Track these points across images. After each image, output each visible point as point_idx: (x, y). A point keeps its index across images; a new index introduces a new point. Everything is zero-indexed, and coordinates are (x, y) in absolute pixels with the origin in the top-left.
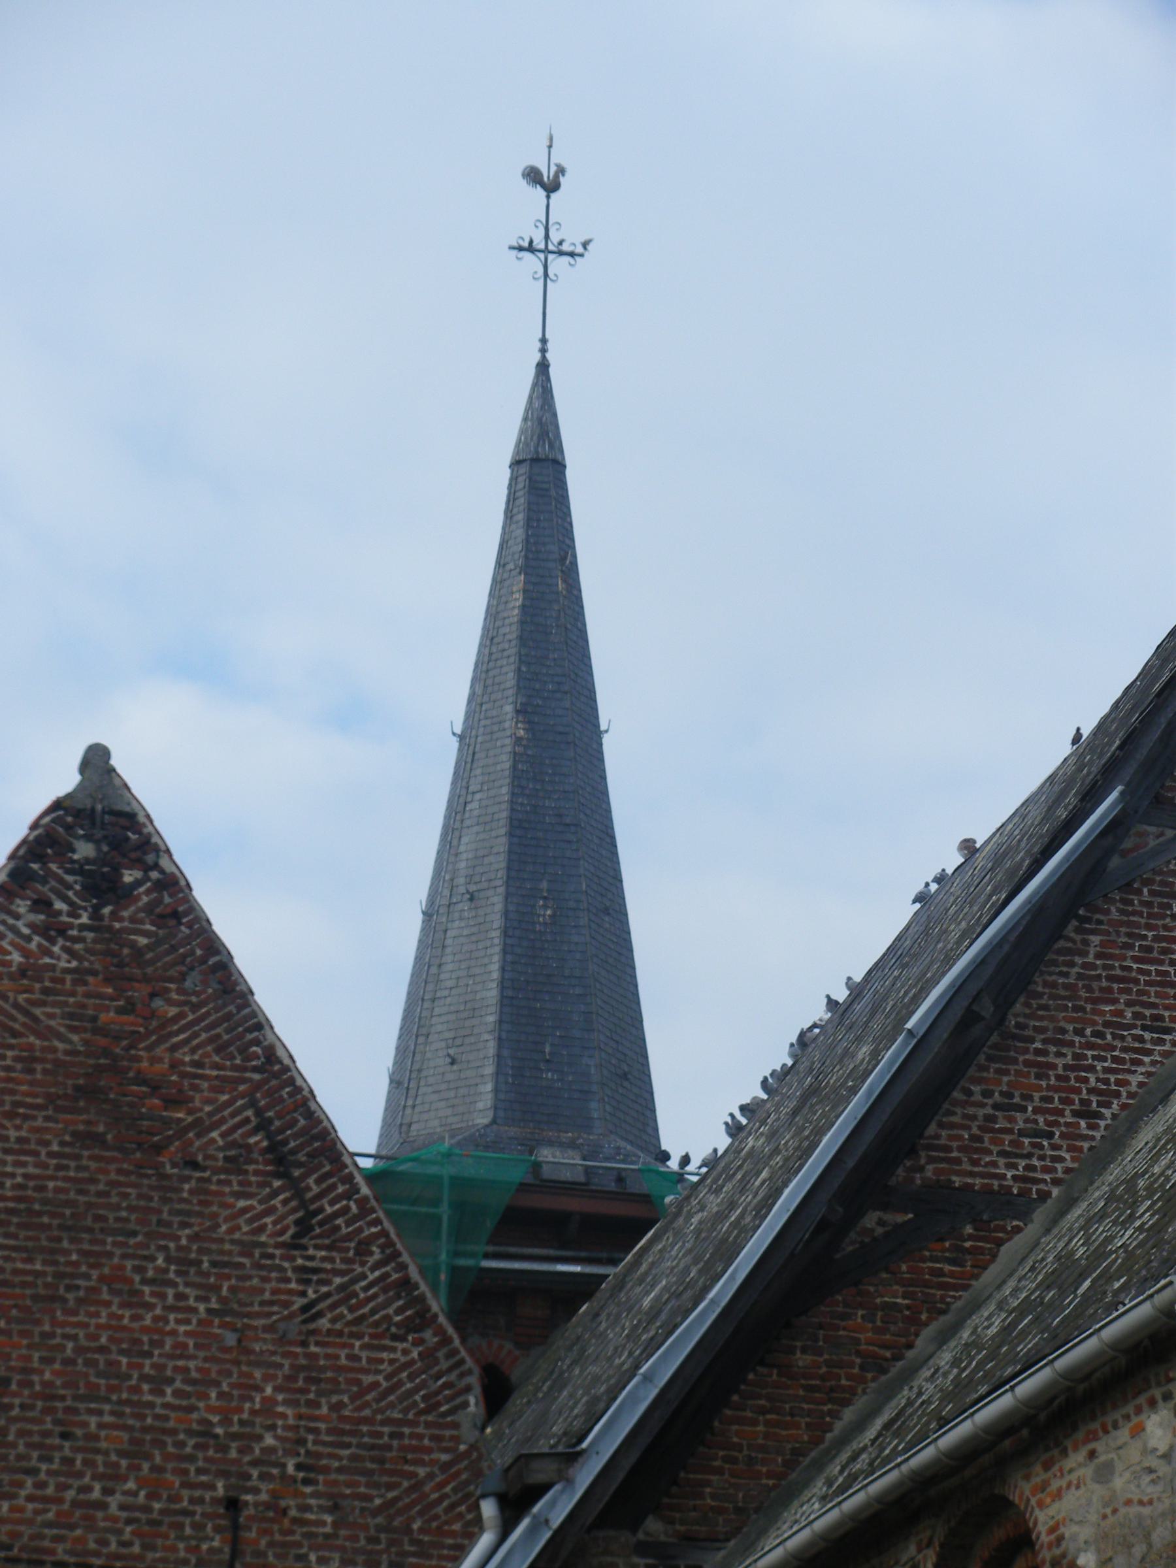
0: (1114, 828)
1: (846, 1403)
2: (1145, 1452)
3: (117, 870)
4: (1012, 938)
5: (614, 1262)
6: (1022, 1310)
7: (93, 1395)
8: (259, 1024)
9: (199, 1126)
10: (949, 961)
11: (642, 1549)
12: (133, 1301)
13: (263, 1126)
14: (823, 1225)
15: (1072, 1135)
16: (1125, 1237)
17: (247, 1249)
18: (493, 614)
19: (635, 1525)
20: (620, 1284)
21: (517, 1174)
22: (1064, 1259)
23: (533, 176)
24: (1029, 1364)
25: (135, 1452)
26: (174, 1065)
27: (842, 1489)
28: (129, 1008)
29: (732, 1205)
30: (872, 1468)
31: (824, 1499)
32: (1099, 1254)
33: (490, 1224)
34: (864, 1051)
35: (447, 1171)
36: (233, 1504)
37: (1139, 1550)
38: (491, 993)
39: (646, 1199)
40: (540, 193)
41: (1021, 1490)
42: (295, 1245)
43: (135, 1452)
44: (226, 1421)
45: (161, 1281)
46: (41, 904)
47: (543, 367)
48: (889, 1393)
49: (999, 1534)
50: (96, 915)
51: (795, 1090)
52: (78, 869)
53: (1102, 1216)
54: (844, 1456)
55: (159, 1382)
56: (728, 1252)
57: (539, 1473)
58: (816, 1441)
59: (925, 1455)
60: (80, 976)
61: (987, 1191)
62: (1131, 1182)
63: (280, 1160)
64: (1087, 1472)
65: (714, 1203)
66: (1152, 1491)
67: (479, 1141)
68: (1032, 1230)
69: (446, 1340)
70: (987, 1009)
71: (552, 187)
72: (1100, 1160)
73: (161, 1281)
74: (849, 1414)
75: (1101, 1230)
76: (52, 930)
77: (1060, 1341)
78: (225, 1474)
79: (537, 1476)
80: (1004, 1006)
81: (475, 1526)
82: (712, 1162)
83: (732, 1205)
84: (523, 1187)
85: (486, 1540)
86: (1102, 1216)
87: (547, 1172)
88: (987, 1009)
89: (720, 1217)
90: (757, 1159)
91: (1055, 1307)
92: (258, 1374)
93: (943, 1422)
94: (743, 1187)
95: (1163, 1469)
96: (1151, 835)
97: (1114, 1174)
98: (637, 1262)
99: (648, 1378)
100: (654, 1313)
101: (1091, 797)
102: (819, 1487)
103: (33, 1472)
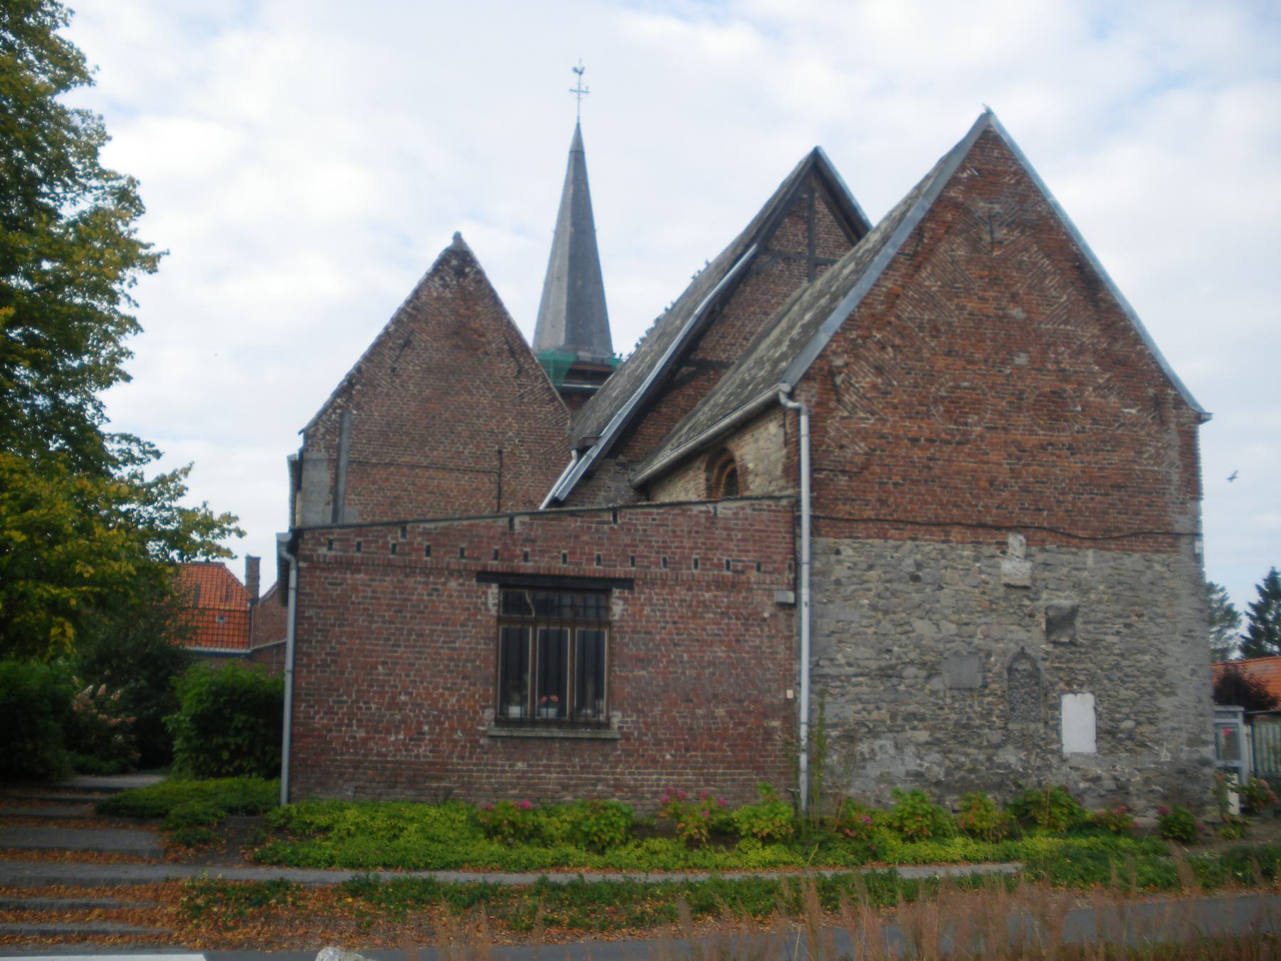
0: (754, 257)
1: (676, 422)
2: (769, 434)
3: (464, 268)
4: (916, 214)
5: (601, 384)
6: (731, 394)
7: (459, 421)
8: (505, 313)
9: (489, 343)
10: (705, 295)
11: (618, 464)
12: (470, 393)
13: (507, 342)
14: (670, 371)
15: (741, 345)
16: (762, 373)
17: (503, 378)
18: (564, 196)
19: (616, 457)
20: (604, 390)
21: (571, 359)
22: (743, 380)
23: (575, 70)
24: (735, 410)
25: (472, 437)
26: (481, 325)
27: (678, 447)
28: (468, 309)
29: (639, 367)
30: (687, 441)
31: (672, 450)
32: (754, 378)
33: (564, 373)
34: (678, 322)
35: (552, 358)
36: (500, 452)
37: (766, 462)
38: (564, 307)
39: (609, 366)
40: (577, 75)
41: (732, 445)
42: (517, 377)
43: (472, 437)
44: (498, 427)
45: (478, 388)
46: (442, 278)
47: (578, 125)
48: (689, 420)
49: (724, 458)
50: (458, 281)
51: (656, 334)
52: (453, 268)
53: (753, 368)
54: (676, 438)
55: (478, 417)
56: (640, 380)
57: (588, 443)
58: (668, 433)
59: (703, 436)
60: (453, 299)
61: (717, 362)
62: (762, 358)
63: (512, 353)
64: (751, 440)
65: (633, 366)
66: (770, 445)
67: (561, 350)
68: (730, 372)
69: (561, 405)
70: (718, 308)
71: (581, 73)
72: (750, 352)
73: (478, 388)
74: (677, 426)
75: (753, 372)
76: (445, 286)
77: (744, 403)
78: (498, 443)
79: (588, 444)
80: (722, 308)
81: (570, 458)
82: (630, 356)
83: (639, 367)
84: (574, 363)
85: (573, 462)
86: (753, 368)
87: (581, 359)
88: (718, 308)
89: (635, 370)
90: (646, 354)
91: (741, 393)
92: (507, 415)
93: (709, 427)
94: (642, 362)
95: (774, 439)
96: (764, 258)
97: (755, 356)
98: (609, 383)
99: (620, 415)
100: (616, 398)
101: (747, 247)
102: (669, 446)
103: (443, 443)
